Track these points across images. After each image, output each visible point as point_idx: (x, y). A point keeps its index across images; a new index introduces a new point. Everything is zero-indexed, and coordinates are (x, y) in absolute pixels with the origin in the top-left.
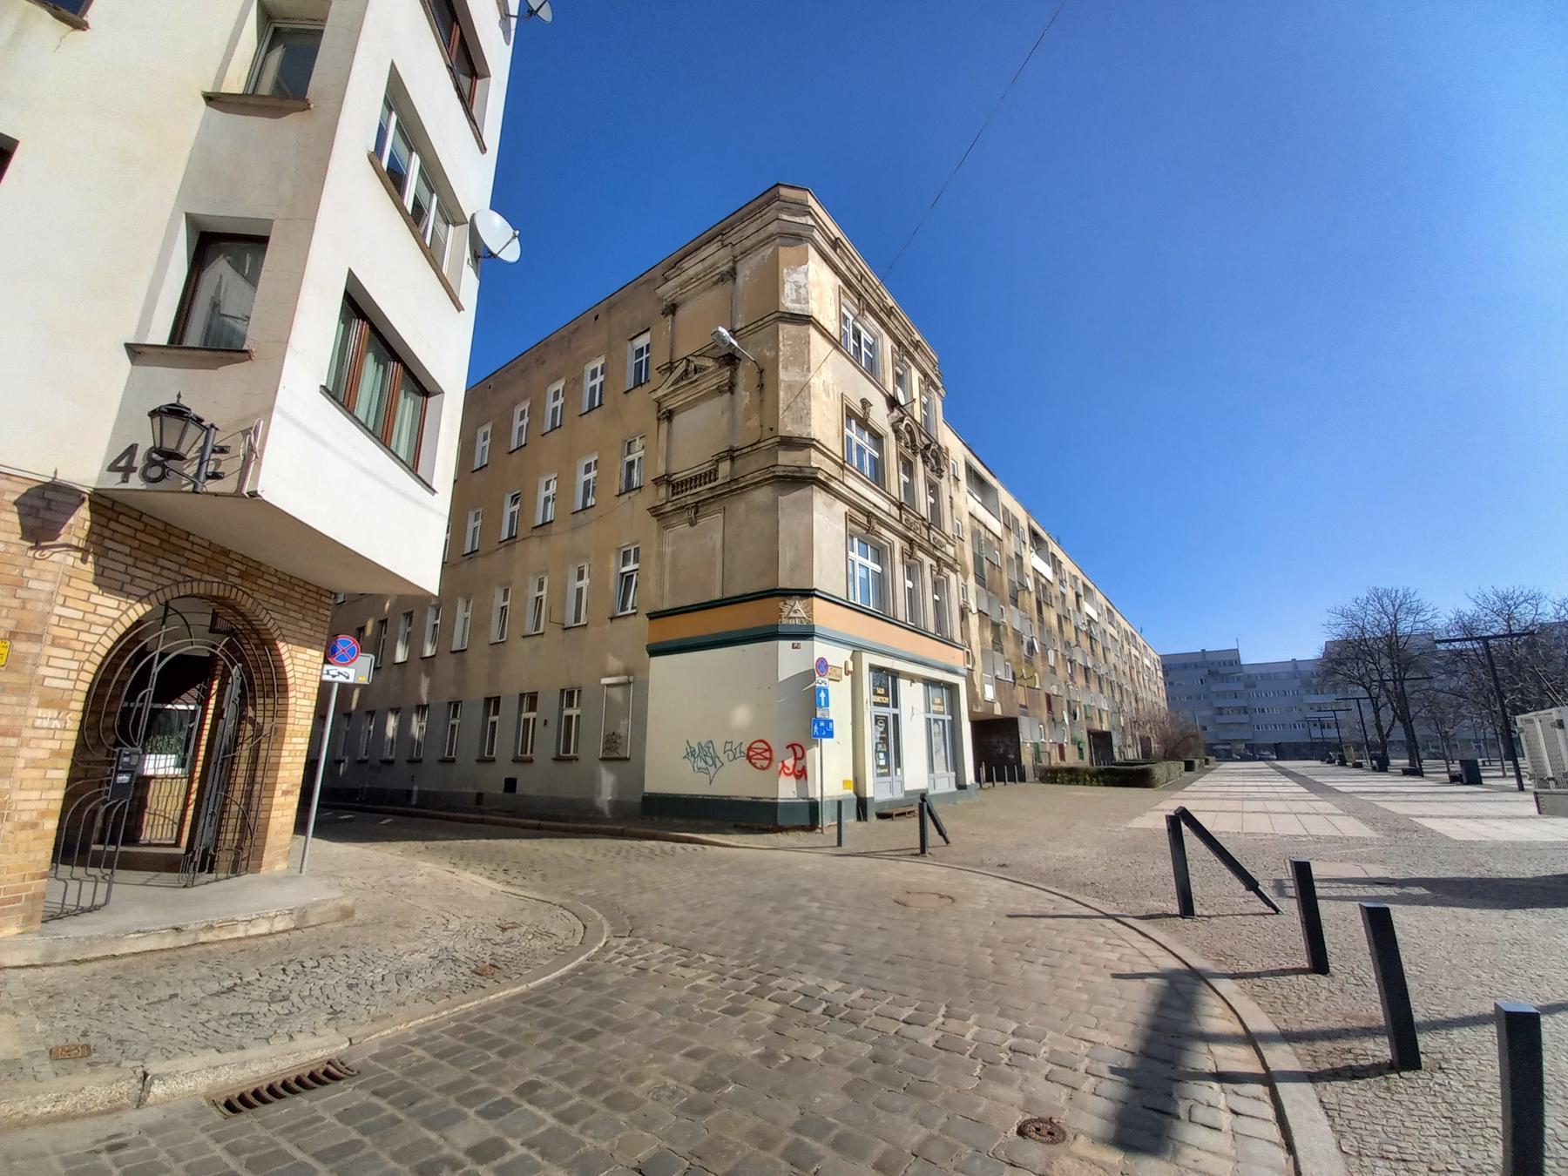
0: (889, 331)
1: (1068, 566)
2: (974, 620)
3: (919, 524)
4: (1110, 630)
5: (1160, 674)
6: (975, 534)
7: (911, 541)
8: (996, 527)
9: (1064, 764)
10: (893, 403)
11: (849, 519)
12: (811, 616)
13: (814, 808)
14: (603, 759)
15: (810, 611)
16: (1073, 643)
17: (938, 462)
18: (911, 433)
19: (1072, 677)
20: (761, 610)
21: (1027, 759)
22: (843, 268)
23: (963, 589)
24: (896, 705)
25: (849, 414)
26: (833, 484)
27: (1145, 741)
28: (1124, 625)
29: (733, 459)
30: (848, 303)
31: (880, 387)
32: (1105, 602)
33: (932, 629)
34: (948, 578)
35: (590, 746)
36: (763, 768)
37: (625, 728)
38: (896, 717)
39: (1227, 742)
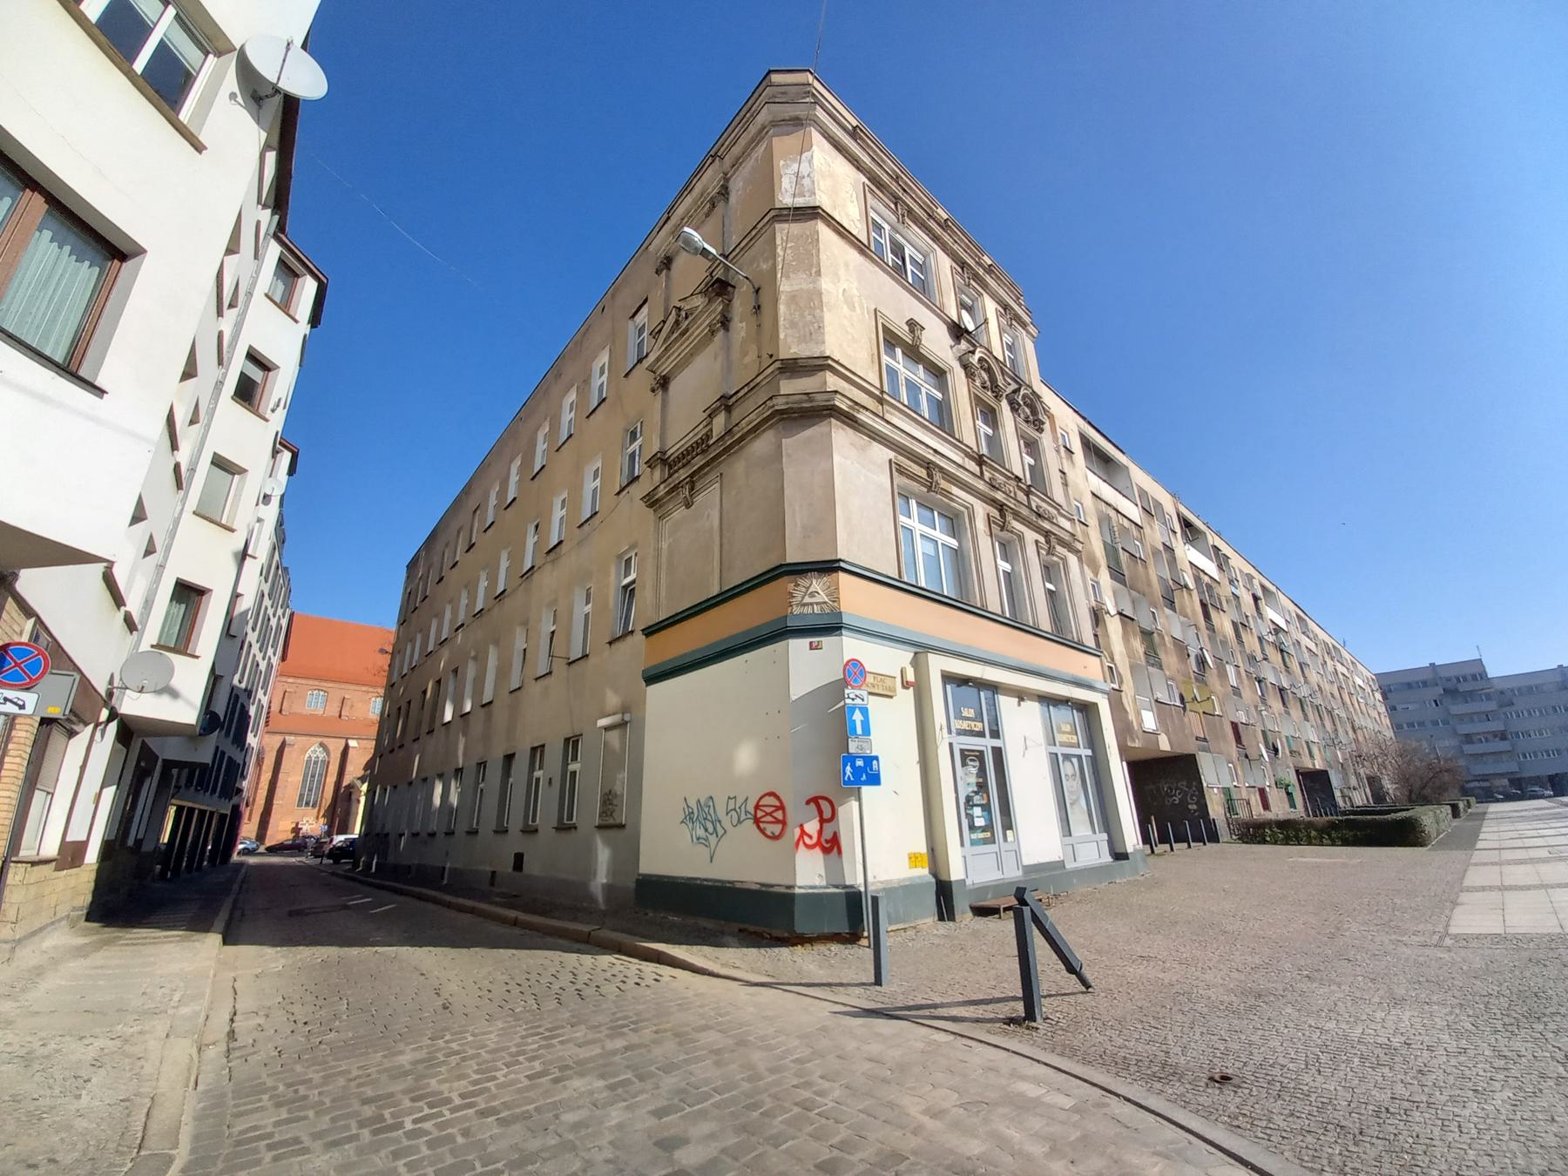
0: (945, 248)
1: (1236, 561)
2: (1114, 626)
3: (1011, 486)
4: (1305, 641)
5: (1378, 696)
6: (1104, 520)
7: (1001, 507)
8: (1134, 512)
9: (1269, 816)
10: (958, 332)
11: (897, 469)
12: (837, 600)
13: (853, 900)
14: (600, 827)
15: (835, 595)
16: (1259, 657)
17: (1034, 412)
18: (989, 370)
19: (1263, 700)
20: (767, 600)
21: (1216, 810)
22: (867, 160)
23: (1090, 585)
24: (996, 734)
25: (891, 340)
26: (863, 417)
27: (1373, 781)
28: (1322, 635)
29: (728, 409)
30: (881, 208)
31: (939, 312)
32: (1292, 607)
33: (1045, 624)
34: (1064, 560)
35: (587, 812)
36: (775, 837)
37: (621, 784)
38: (998, 753)
39: (1485, 778)
